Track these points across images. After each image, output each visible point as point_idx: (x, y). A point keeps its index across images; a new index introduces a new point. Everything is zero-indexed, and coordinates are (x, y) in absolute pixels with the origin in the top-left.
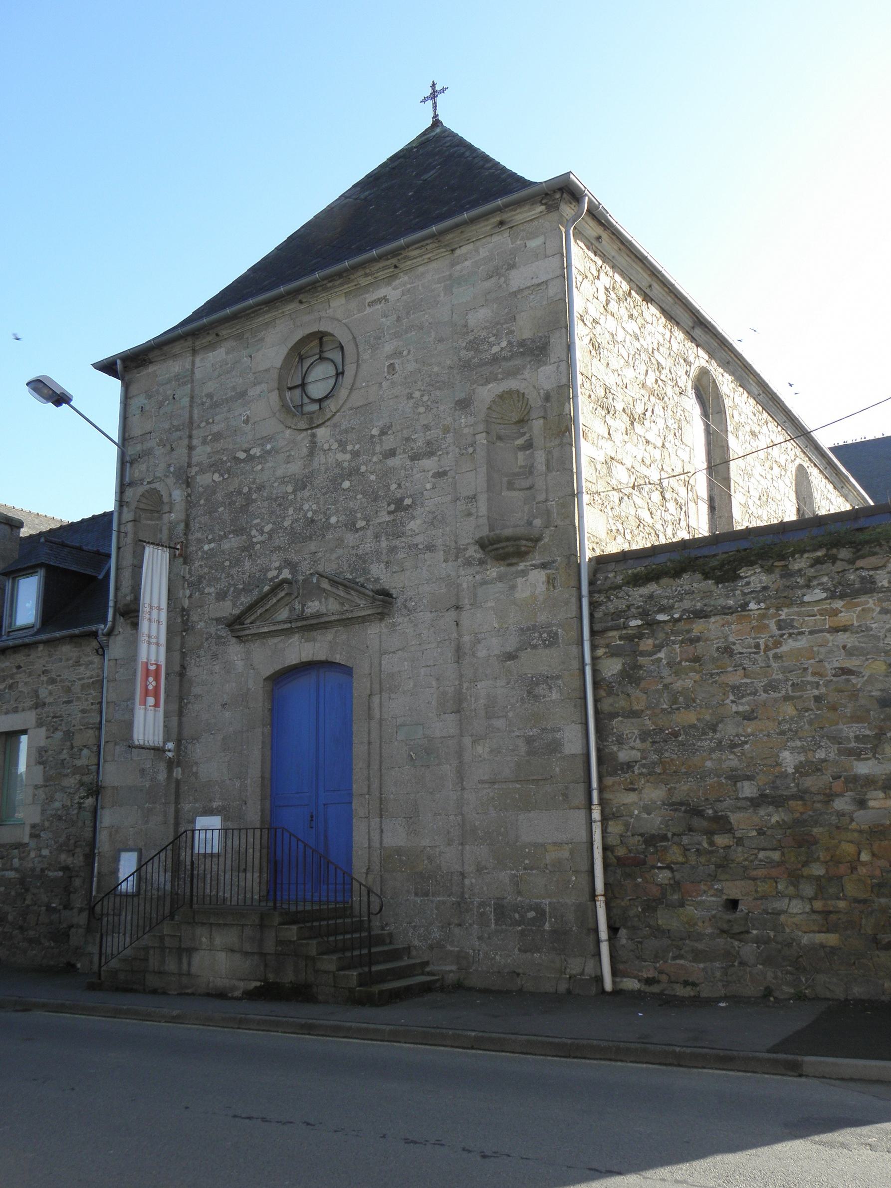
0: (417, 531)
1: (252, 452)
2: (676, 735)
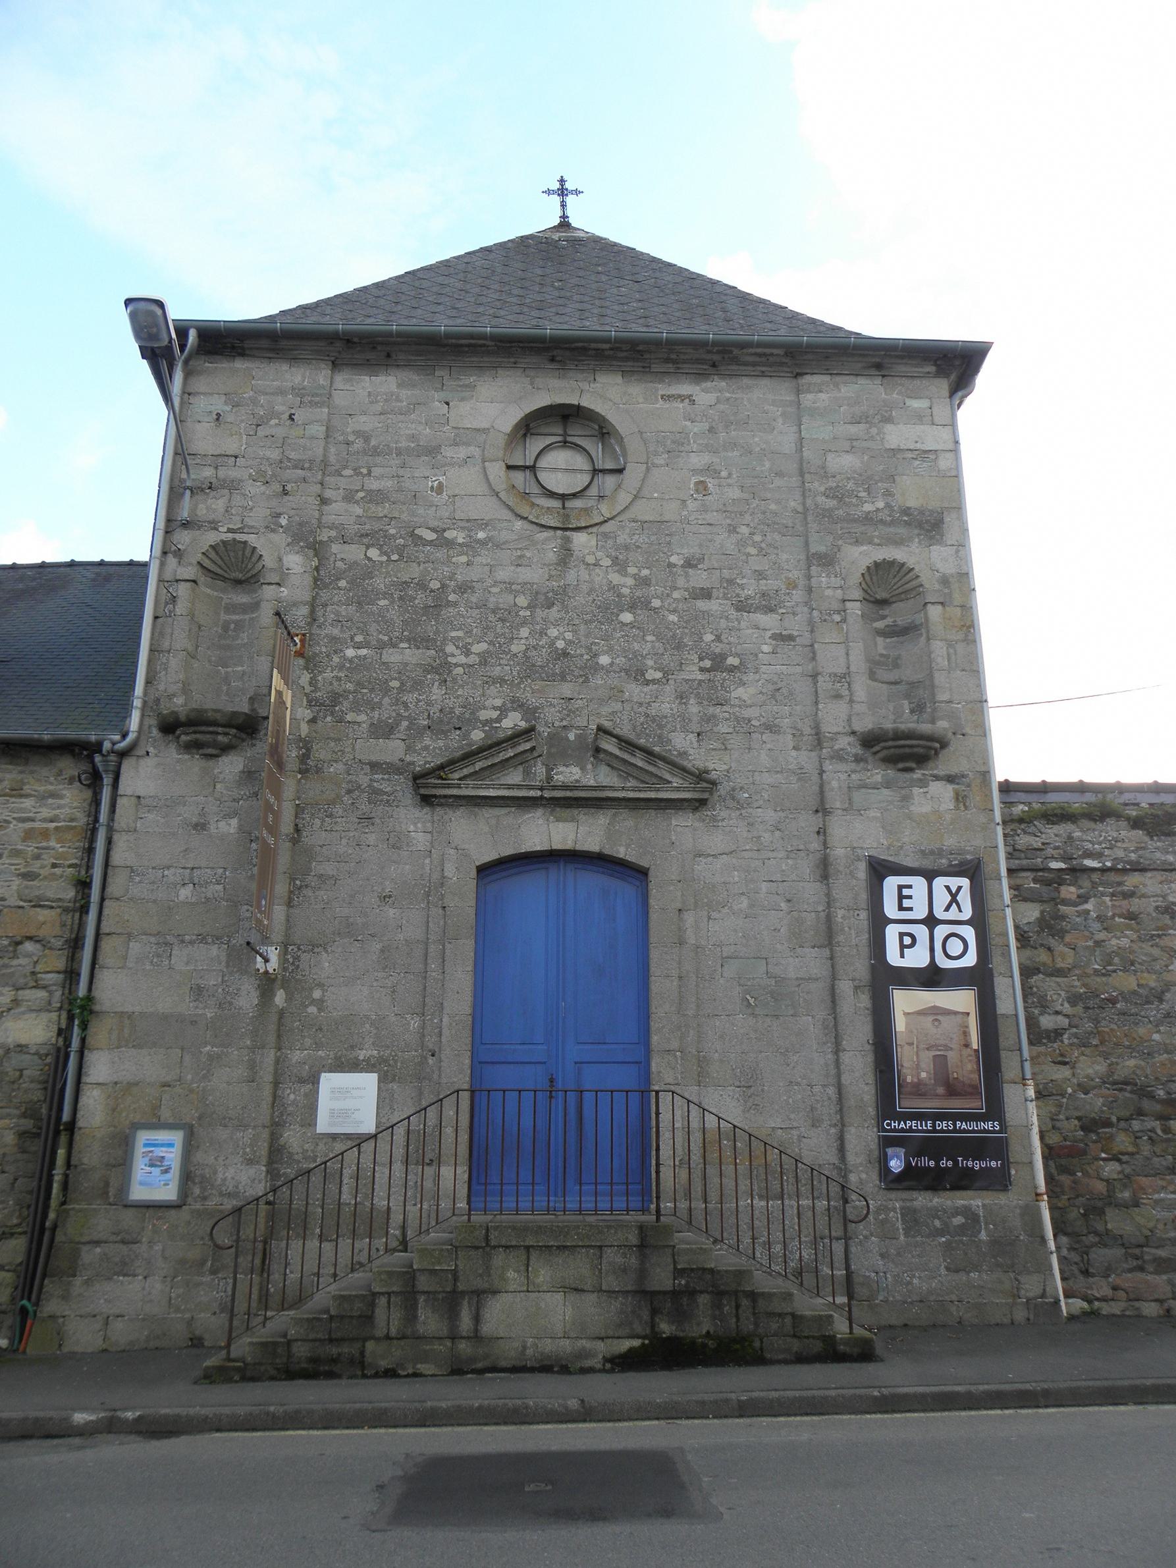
0: (749, 702)
1: (446, 534)
2: (1113, 1001)
